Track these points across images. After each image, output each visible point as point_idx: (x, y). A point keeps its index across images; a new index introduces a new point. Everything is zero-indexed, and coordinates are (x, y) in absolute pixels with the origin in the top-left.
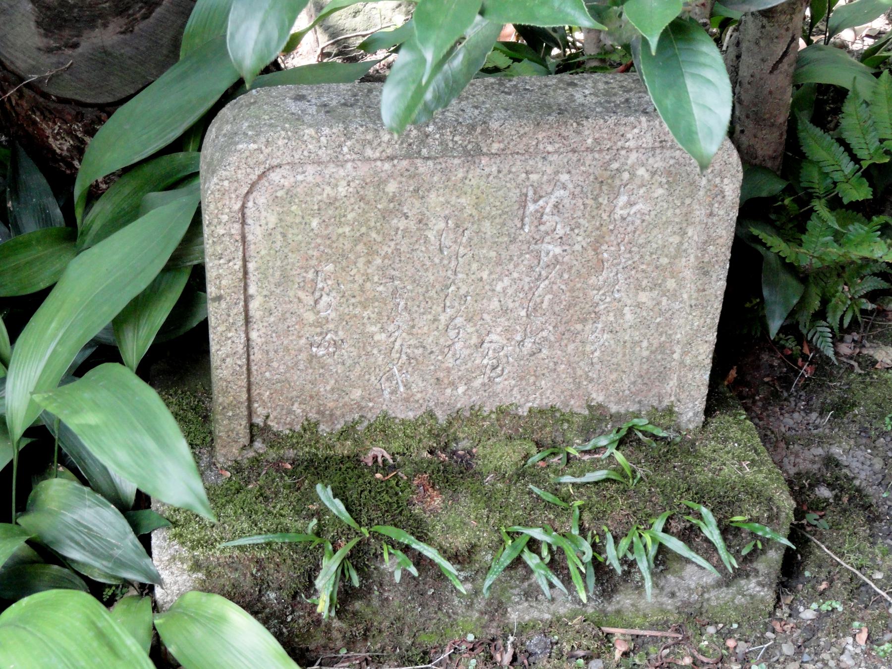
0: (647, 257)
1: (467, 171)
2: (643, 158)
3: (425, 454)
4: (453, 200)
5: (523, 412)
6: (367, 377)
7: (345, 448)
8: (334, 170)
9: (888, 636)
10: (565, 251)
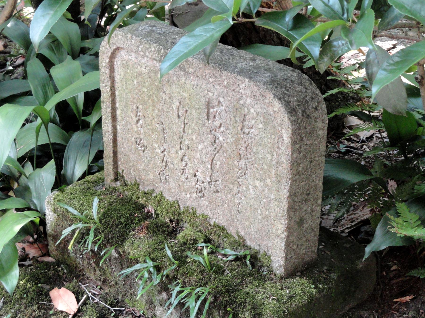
0: (257, 161)
1: (186, 80)
2: (253, 103)
3: (167, 220)
4: (182, 93)
5: (212, 223)
6: (155, 169)
7: (142, 201)
8: (141, 59)
9: (21, 317)
10: (224, 140)
